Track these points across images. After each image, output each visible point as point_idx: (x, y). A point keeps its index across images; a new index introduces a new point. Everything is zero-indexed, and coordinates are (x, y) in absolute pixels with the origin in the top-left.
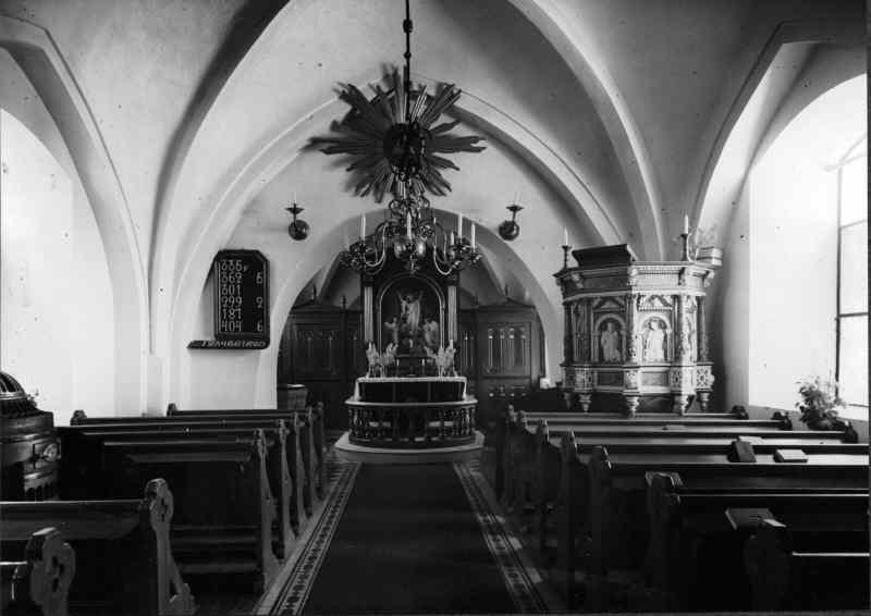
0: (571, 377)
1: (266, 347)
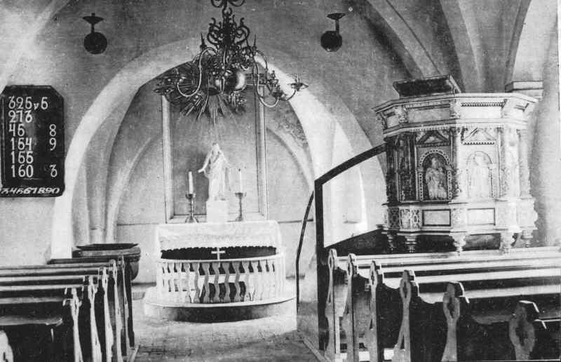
0: (394, 216)
1: (60, 194)
